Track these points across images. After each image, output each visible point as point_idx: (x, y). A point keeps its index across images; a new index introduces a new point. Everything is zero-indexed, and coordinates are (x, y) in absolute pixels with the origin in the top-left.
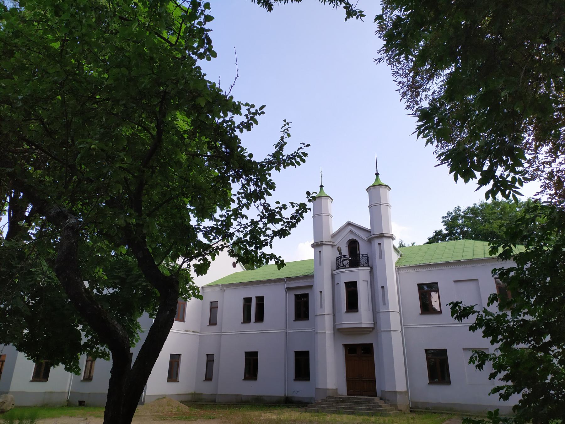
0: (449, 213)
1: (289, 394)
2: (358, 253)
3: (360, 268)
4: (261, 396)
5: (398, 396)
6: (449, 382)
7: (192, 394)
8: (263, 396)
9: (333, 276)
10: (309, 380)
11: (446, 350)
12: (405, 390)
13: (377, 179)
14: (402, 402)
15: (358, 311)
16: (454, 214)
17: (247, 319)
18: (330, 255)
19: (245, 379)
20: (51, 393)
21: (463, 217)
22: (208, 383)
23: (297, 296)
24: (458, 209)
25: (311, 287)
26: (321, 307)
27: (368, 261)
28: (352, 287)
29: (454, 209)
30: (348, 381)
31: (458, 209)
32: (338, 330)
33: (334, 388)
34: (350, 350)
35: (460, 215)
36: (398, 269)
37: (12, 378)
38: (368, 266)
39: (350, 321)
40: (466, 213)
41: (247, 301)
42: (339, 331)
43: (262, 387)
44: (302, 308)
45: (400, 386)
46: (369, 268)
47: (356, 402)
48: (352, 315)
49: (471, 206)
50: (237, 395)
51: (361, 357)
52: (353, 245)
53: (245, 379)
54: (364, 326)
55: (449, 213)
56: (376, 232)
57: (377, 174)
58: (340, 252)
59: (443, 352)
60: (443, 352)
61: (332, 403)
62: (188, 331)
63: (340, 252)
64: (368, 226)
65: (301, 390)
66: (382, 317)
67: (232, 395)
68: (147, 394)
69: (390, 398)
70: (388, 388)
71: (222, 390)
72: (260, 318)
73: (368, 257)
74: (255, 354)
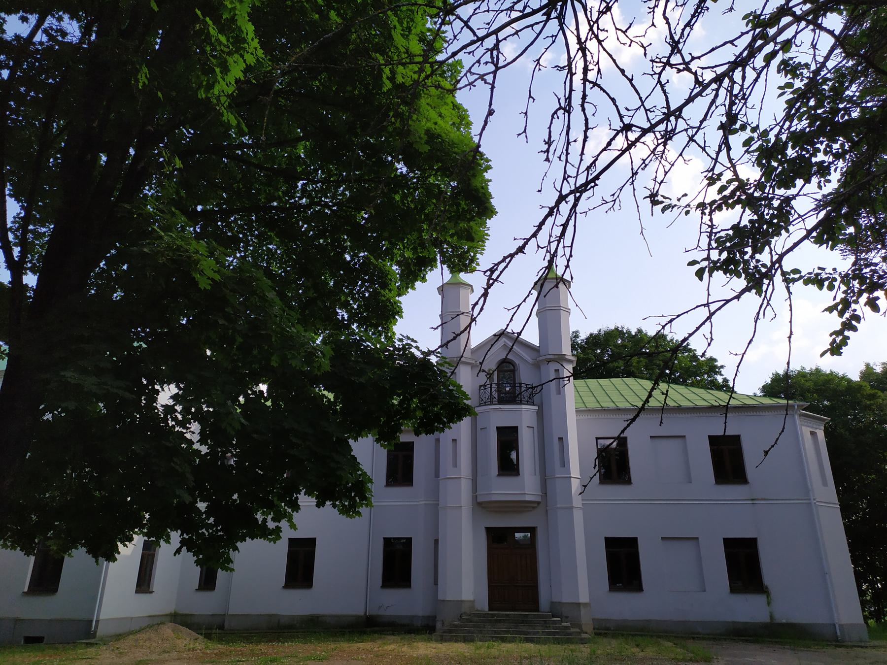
1: (373, 611)
3: (524, 406)
4: (318, 617)
6: (639, 588)
8: (323, 616)
10: (410, 586)
11: (636, 538)
14: (586, 619)
19: (287, 586)
22: (206, 595)
26: (455, 465)
28: (508, 438)
30: (490, 587)
33: (471, 598)
34: (497, 538)
36: (578, 411)
37: (113, 619)
39: (503, 489)
42: (481, 506)
43: (321, 598)
47: (523, 622)
48: (509, 481)
50: (270, 616)
53: (287, 586)
54: (528, 498)
56: (552, 351)
59: (632, 542)
60: (632, 542)
61: (465, 626)
67: (258, 615)
68: (101, 617)
70: (566, 598)
71: (235, 609)
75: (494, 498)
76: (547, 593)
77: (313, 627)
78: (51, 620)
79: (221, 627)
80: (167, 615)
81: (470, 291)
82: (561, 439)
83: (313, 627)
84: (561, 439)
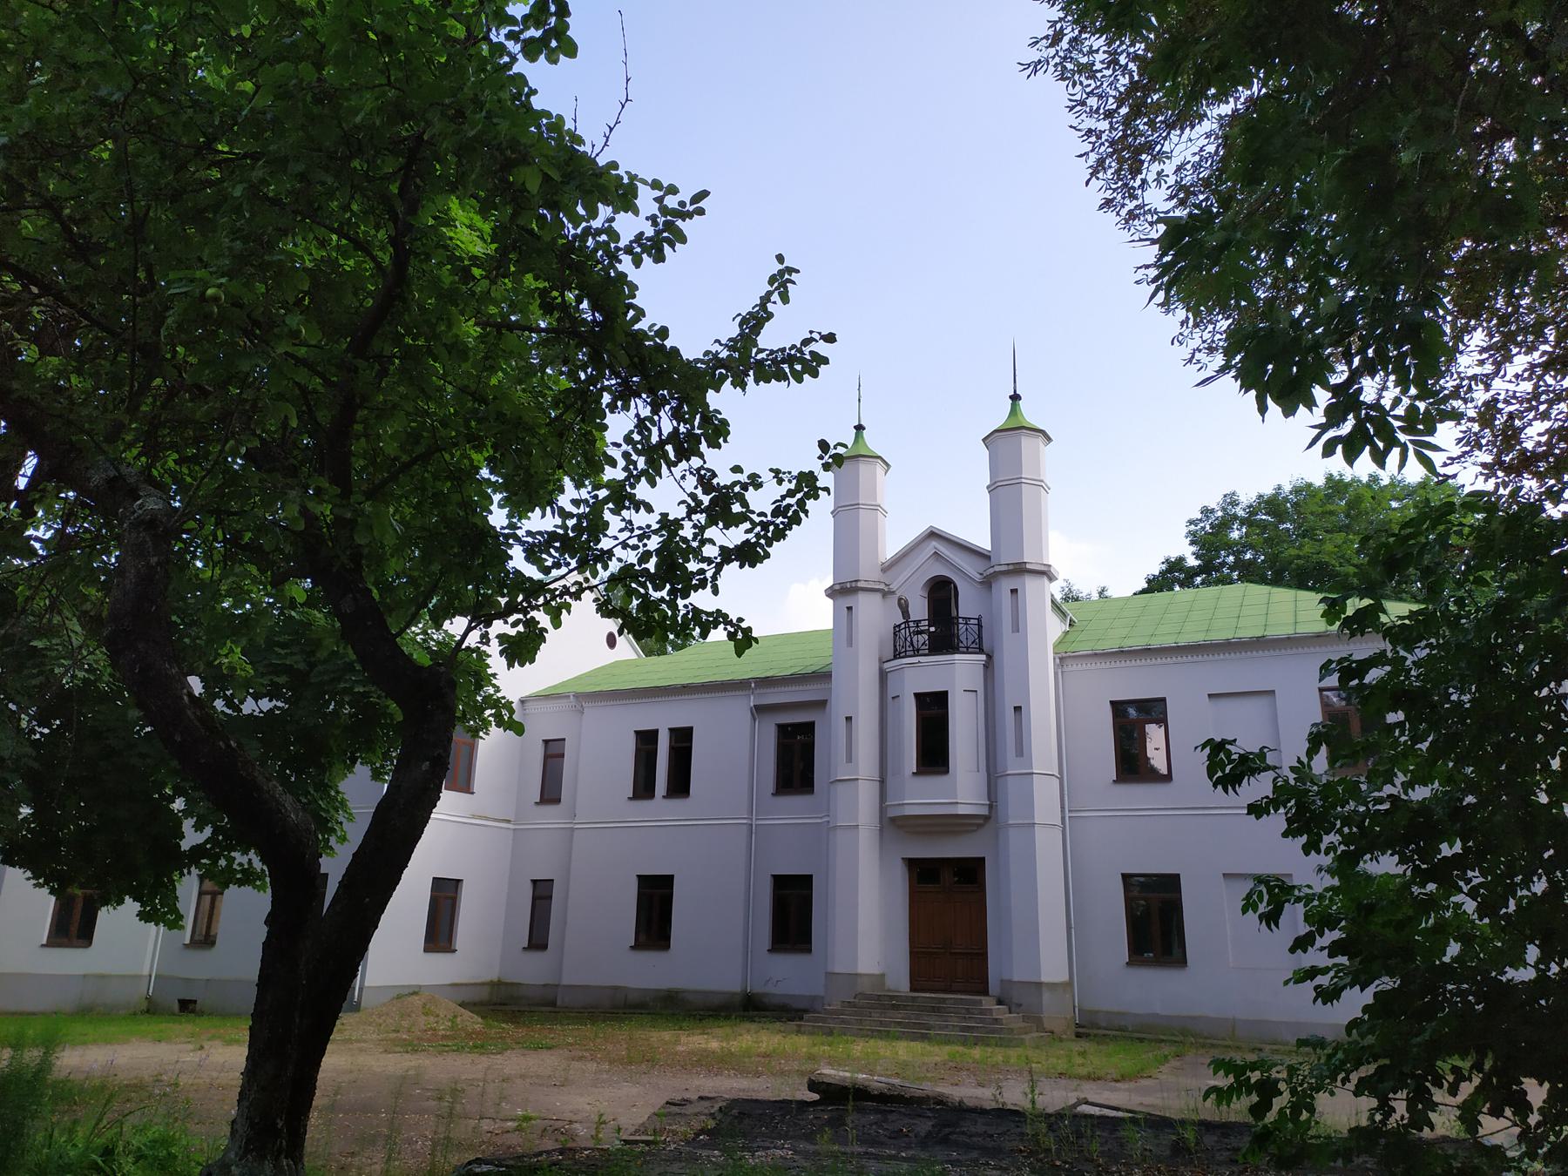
0: (1207, 512)
1: (756, 987)
2: (954, 614)
3: (957, 656)
4: (677, 992)
5: (1046, 996)
7: (492, 984)
9: (883, 676)
10: (810, 951)
12: (1065, 978)
13: (1014, 411)
14: (1055, 1011)
15: (947, 772)
16: (1220, 514)
17: (643, 788)
18: (875, 617)
19: (638, 946)
20: (102, 977)
21: (1243, 522)
22: (536, 957)
23: (783, 729)
24: (1231, 500)
25: (821, 704)
26: (849, 759)
27: (980, 637)
28: (933, 709)
29: (1220, 498)
31: (1231, 500)
32: (893, 820)
33: (876, 971)
34: (922, 873)
35: (1235, 517)
36: (1062, 660)
38: (981, 651)
39: (923, 796)
40: (1252, 510)
41: (647, 740)
42: (895, 825)
44: (796, 762)
45: (1053, 965)
46: (983, 657)
47: (933, 1009)
48: (933, 782)
49: (1268, 491)
50: (616, 988)
51: (950, 892)
52: (941, 592)
53: (638, 946)
54: (962, 810)
55: (1207, 512)
56: (1006, 558)
57: (1015, 398)
58: (905, 613)
59: (1170, 883)
60: (1170, 883)
62: (480, 817)
63: (905, 613)
64: (984, 543)
65: (786, 975)
66: (1011, 788)
69: (1024, 999)
71: (572, 976)
72: (680, 785)
73: (980, 626)
74: (667, 881)
75: (909, 811)
76: (1004, 965)
77: (674, 1007)
78: (84, 976)
79: (553, 1004)
80: (483, 984)
81: (880, 468)
82: (1018, 709)
83: (674, 1007)
84: (1018, 709)
